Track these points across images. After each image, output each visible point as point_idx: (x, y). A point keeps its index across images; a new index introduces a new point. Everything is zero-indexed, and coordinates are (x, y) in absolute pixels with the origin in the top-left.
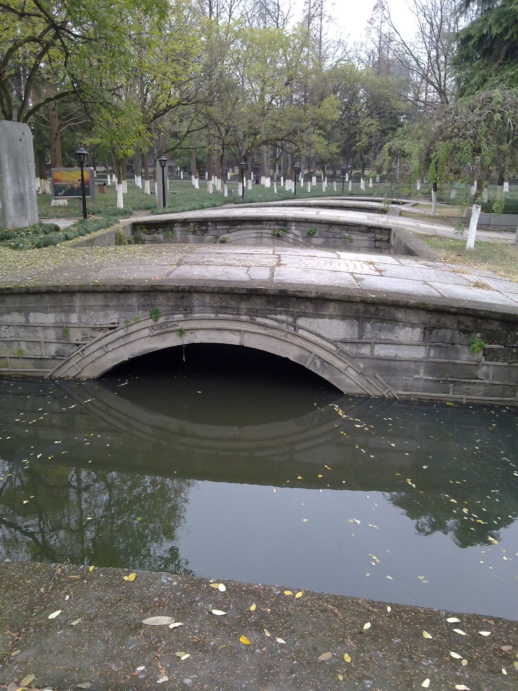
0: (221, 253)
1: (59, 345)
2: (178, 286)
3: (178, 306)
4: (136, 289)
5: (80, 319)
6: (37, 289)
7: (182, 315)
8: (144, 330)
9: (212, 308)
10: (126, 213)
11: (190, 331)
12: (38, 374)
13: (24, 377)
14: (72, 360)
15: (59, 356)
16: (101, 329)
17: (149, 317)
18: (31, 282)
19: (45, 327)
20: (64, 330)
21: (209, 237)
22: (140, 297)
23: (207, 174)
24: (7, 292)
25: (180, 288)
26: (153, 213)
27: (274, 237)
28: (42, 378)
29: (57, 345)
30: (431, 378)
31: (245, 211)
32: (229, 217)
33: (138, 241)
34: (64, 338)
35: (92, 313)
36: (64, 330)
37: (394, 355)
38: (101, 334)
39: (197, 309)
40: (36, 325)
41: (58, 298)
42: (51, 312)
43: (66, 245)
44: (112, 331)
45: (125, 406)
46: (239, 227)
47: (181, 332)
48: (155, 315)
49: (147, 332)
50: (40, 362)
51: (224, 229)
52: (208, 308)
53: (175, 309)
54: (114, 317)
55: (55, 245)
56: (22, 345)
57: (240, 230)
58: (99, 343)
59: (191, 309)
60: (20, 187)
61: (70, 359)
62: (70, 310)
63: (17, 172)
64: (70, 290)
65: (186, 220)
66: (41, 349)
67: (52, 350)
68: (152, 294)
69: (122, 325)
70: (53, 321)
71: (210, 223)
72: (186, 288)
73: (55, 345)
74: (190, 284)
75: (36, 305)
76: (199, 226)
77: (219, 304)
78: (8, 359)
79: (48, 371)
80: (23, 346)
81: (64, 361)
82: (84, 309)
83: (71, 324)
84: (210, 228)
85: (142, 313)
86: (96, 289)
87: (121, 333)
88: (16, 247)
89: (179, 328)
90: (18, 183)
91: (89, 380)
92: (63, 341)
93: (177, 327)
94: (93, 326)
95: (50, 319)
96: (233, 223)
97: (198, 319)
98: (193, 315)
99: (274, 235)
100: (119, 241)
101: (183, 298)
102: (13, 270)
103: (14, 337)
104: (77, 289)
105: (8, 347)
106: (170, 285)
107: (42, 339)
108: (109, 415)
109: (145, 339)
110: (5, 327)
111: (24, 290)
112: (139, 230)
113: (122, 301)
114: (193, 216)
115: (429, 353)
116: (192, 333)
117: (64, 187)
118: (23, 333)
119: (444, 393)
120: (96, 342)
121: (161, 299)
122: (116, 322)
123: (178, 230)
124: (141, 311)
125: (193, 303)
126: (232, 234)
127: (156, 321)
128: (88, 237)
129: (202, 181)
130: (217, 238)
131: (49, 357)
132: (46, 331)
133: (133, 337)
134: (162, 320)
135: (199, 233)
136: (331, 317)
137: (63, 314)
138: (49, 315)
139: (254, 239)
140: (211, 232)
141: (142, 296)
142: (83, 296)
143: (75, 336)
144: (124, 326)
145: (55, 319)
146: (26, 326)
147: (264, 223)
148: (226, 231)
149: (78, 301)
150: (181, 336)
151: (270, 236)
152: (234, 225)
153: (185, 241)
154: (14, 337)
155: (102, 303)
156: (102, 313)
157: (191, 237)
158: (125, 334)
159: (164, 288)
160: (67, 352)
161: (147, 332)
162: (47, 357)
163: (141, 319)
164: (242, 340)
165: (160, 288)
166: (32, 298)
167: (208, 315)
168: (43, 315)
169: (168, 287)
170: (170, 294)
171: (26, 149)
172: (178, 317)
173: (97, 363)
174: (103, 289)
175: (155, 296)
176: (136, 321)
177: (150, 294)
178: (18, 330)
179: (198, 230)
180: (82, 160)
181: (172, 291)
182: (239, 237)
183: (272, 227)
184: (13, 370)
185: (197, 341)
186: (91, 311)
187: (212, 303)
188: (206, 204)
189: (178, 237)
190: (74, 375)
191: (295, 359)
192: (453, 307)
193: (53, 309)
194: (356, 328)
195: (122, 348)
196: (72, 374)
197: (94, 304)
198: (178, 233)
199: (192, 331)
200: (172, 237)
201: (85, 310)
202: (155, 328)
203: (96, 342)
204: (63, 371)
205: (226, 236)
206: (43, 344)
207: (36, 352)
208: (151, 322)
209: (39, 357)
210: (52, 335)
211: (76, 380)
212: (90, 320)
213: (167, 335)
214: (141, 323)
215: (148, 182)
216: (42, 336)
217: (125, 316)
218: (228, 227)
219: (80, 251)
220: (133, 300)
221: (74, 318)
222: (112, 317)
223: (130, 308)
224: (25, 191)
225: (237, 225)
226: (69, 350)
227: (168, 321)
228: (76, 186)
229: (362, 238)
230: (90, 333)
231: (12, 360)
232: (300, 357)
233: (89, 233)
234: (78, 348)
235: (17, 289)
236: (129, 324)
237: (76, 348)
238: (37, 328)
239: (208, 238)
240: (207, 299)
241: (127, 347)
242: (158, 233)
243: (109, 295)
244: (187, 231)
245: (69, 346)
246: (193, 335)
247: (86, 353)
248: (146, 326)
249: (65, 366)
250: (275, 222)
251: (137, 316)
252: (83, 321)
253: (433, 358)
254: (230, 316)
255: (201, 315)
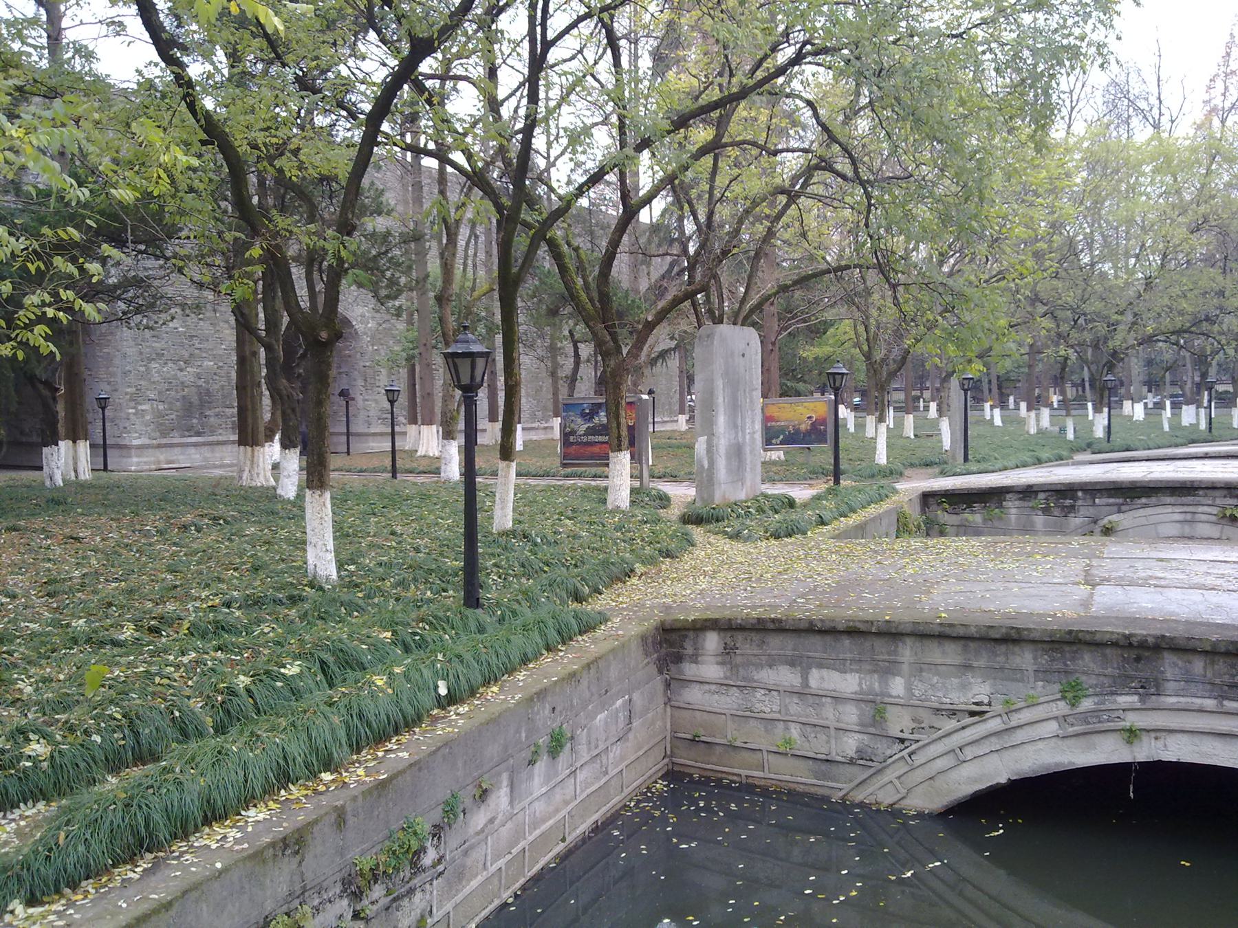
0: (1168, 560)
1: (865, 737)
2: (1131, 635)
3: (1127, 676)
4: (1033, 635)
5: (909, 689)
6: (828, 625)
7: (1136, 698)
8: (1045, 724)
9: (1209, 687)
10: (891, 473)
11: (1153, 735)
12: (820, 791)
13: (790, 793)
14: (888, 771)
15: (862, 758)
16: (953, 713)
17: (1059, 696)
18: (808, 609)
19: (838, 699)
20: (876, 710)
21: (1078, 521)
22: (1040, 653)
23: (1011, 399)
24: (772, 626)
25: (1134, 640)
26: (943, 473)
27: (1223, 521)
28: (826, 799)
29: (861, 736)
31: (1145, 469)
32: (1122, 482)
33: (932, 529)
34: (874, 723)
35: (935, 679)
36: (876, 710)
38: (952, 724)
39: (1171, 685)
40: (821, 693)
41: (868, 644)
42: (852, 671)
43: (822, 534)
44: (976, 719)
45: (998, 882)
46: (1144, 500)
47: (1132, 735)
48: (1072, 693)
49: (1052, 727)
50: (824, 767)
51: (1108, 505)
52: (1201, 686)
53: (1120, 684)
54: (980, 690)
55: (805, 533)
56: (793, 730)
57: (1146, 506)
58: (946, 740)
59: (1157, 686)
60: (737, 433)
61: (884, 768)
62: (889, 669)
64: (893, 631)
65: (1030, 486)
66: (828, 742)
67: (850, 745)
68: (1067, 648)
69: (998, 708)
70: (856, 688)
71: (1080, 494)
72: (1150, 639)
73: (857, 736)
74: (1158, 633)
75: (825, 656)
76: (1057, 499)
77: (1226, 678)
78: (765, 754)
79: (839, 787)
80: (795, 732)
81: (872, 771)
82: (919, 668)
83: (891, 696)
84: (1080, 503)
85: (1043, 687)
86: (948, 631)
87: (994, 724)
88: (736, 536)
89: (1127, 724)
90: (735, 426)
91: (920, 815)
92: (872, 730)
93: (1123, 723)
94: (937, 705)
95: (849, 683)
96: (1131, 493)
97: (1179, 710)
98: (1162, 699)
99: (1224, 516)
100: (902, 528)
101: (1138, 659)
102: (758, 580)
103: (780, 712)
104: (909, 629)
105: (767, 731)
106: (1112, 633)
107: (832, 723)
108: (961, 894)
109: (1044, 740)
110: (763, 692)
111: (804, 625)
112: (934, 507)
113: (1001, 659)
114: (1041, 480)
116: (1156, 738)
117: (782, 430)
118: (795, 707)
120: (940, 738)
121: (1088, 660)
122: (986, 701)
123: (1013, 508)
124: (1040, 683)
125: (1163, 672)
126: (1126, 515)
127: (1073, 705)
128: (852, 520)
129: (1007, 413)
130: (1095, 522)
131: (843, 760)
132: (840, 708)
133: (1020, 736)
134: (1087, 704)
135: (1056, 512)
137: (876, 676)
138: (848, 676)
139: (1178, 525)
140: (1083, 511)
141: (1045, 651)
142: (918, 644)
143: (899, 722)
144: (1002, 712)
145: (860, 684)
146: (803, 694)
147: (1201, 493)
148: (1115, 508)
149: (907, 652)
150: (1129, 742)
151: (1214, 518)
152: (1132, 498)
153: (1027, 529)
154: (780, 712)
155: (958, 660)
156: (955, 681)
157: (1039, 520)
158: (1003, 727)
159: (1098, 637)
160: (880, 752)
161: (1052, 727)
162: (839, 759)
163: (1042, 699)
165: (1088, 637)
166: (816, 640)
167: (1198, 701)
168: (835, 675)
169: (1108, 636)
170: (1108, 651)
171: (751, 369)
172: (1124, 700)
173: (938, 782)
174: (962, 631)
175: (1076, 652)
176: (1030, 702)
177: (1066, 649)
178: (787, 700)
179: (1056, 506)
180: (837, 384)
181: (1115, 644)
183: (1218, 501)
184: (772, 776)
185: (1169, 756)
186: (934, 675)
187: (1209, 674)
188: (1044, 455)
189: (1013, 517)
190: (889, 801)
193: (857, 664)
195: (995, 755)
196: (886, 798)
197: (939, 661)
198: (1014, 511)
199: (1158, 734)
200: (1000, 519)
201: (921, 670)
202: (1070, 720)
203: (940, 738)
204: (870, 790)
205: (1114, 518)
206: (832, 731)
207: (819, 746)
208: (1062, 708)
209: (824, 757)
210: (851, 714)
211: (894, 812)
212: (930, 692)
213: (1097, 739)
214: (1041, 707)
215: (911, 416)
216: (831, 717)
217: (1005, 691)
218: (1121, 501)
219: (859, 546)
220: (1025, 659)
221: (897, 686)
222: (976, 689)
223: (1017, 674)
225: (1139, 498)
226: (883, 748)
227: (1103, 707)
228: (803, 427)
230: (928, 718)
231: (772, 757)
233: (855, 511)
234: (903, 746)
235: (791, 622)
236: (1013, 708)
237: (898, 746)
238: (824, 699)
239: (1075, 521)
240: (1198, 665)
241: (1005, 754)
242: (973, 512)
243: (972, 645)
244: (1032, 507)
245: (884, 740)
246: (1160, 744)
247: (919, 759)
248: (1051, 715)
249: (874, 780)
250: (1225, 492)
251: (1032, 692)
252: (916, 693)
255: (1182, 699)
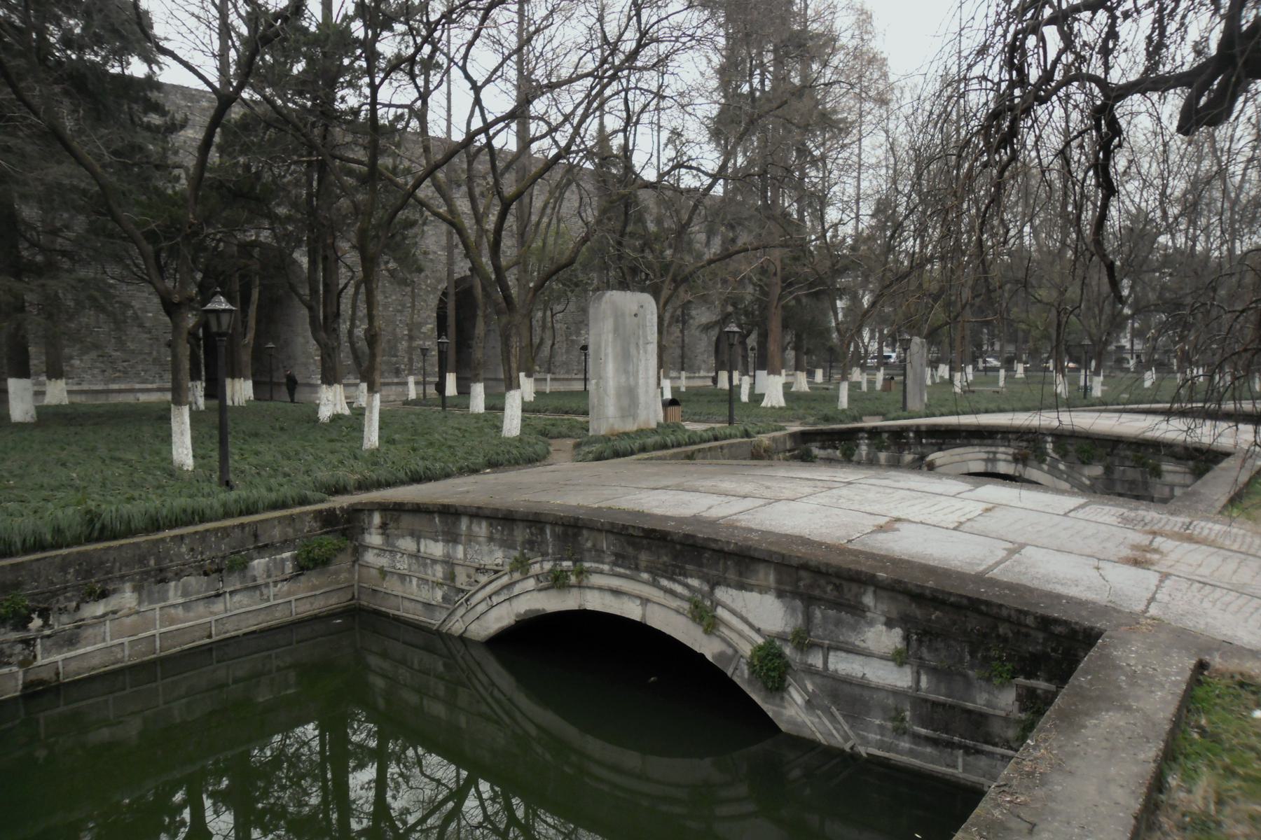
30: (923, 731)
33: (806, 458)
37: (860, 675)
60: (628, 379)
63: (626, 358)
95: (436, 549)
115: (918, 682)
119: (948, 766)
136: (763, 590)
153: (872, 463)
164: (644, 616)
182: (957, 458)
191: (713, 658)
192: (950, 594)
194: (800, 616)
195: (507, 604)
224: (637, 383)
229: (1178, 469)
232: (721, 655)
253: (928, 691)
254: (628, 572)
